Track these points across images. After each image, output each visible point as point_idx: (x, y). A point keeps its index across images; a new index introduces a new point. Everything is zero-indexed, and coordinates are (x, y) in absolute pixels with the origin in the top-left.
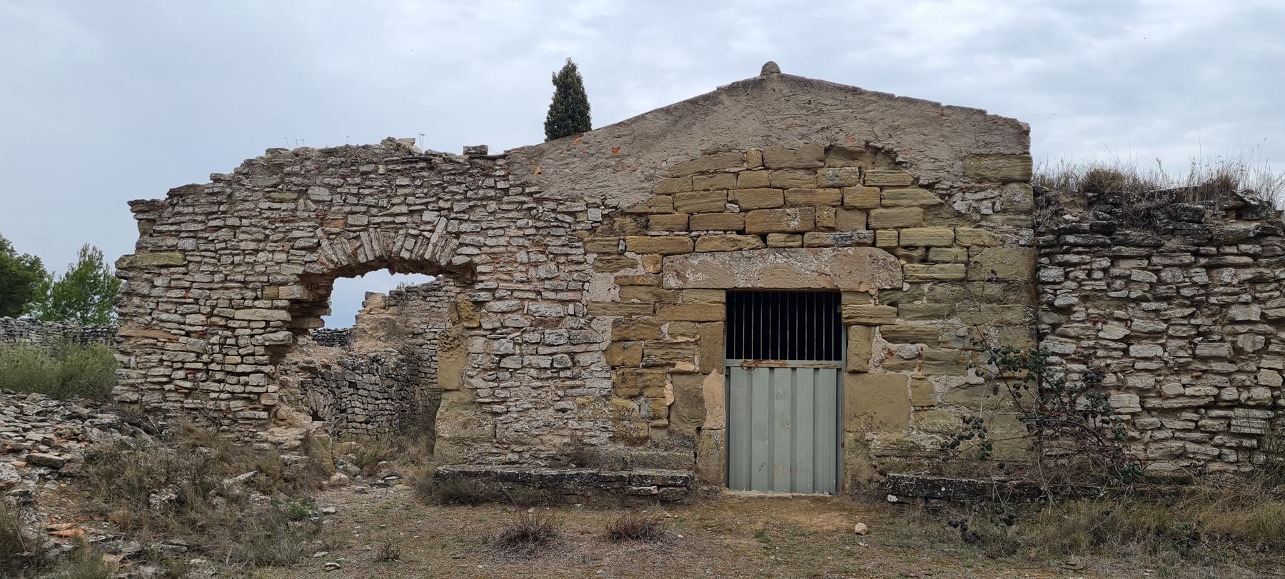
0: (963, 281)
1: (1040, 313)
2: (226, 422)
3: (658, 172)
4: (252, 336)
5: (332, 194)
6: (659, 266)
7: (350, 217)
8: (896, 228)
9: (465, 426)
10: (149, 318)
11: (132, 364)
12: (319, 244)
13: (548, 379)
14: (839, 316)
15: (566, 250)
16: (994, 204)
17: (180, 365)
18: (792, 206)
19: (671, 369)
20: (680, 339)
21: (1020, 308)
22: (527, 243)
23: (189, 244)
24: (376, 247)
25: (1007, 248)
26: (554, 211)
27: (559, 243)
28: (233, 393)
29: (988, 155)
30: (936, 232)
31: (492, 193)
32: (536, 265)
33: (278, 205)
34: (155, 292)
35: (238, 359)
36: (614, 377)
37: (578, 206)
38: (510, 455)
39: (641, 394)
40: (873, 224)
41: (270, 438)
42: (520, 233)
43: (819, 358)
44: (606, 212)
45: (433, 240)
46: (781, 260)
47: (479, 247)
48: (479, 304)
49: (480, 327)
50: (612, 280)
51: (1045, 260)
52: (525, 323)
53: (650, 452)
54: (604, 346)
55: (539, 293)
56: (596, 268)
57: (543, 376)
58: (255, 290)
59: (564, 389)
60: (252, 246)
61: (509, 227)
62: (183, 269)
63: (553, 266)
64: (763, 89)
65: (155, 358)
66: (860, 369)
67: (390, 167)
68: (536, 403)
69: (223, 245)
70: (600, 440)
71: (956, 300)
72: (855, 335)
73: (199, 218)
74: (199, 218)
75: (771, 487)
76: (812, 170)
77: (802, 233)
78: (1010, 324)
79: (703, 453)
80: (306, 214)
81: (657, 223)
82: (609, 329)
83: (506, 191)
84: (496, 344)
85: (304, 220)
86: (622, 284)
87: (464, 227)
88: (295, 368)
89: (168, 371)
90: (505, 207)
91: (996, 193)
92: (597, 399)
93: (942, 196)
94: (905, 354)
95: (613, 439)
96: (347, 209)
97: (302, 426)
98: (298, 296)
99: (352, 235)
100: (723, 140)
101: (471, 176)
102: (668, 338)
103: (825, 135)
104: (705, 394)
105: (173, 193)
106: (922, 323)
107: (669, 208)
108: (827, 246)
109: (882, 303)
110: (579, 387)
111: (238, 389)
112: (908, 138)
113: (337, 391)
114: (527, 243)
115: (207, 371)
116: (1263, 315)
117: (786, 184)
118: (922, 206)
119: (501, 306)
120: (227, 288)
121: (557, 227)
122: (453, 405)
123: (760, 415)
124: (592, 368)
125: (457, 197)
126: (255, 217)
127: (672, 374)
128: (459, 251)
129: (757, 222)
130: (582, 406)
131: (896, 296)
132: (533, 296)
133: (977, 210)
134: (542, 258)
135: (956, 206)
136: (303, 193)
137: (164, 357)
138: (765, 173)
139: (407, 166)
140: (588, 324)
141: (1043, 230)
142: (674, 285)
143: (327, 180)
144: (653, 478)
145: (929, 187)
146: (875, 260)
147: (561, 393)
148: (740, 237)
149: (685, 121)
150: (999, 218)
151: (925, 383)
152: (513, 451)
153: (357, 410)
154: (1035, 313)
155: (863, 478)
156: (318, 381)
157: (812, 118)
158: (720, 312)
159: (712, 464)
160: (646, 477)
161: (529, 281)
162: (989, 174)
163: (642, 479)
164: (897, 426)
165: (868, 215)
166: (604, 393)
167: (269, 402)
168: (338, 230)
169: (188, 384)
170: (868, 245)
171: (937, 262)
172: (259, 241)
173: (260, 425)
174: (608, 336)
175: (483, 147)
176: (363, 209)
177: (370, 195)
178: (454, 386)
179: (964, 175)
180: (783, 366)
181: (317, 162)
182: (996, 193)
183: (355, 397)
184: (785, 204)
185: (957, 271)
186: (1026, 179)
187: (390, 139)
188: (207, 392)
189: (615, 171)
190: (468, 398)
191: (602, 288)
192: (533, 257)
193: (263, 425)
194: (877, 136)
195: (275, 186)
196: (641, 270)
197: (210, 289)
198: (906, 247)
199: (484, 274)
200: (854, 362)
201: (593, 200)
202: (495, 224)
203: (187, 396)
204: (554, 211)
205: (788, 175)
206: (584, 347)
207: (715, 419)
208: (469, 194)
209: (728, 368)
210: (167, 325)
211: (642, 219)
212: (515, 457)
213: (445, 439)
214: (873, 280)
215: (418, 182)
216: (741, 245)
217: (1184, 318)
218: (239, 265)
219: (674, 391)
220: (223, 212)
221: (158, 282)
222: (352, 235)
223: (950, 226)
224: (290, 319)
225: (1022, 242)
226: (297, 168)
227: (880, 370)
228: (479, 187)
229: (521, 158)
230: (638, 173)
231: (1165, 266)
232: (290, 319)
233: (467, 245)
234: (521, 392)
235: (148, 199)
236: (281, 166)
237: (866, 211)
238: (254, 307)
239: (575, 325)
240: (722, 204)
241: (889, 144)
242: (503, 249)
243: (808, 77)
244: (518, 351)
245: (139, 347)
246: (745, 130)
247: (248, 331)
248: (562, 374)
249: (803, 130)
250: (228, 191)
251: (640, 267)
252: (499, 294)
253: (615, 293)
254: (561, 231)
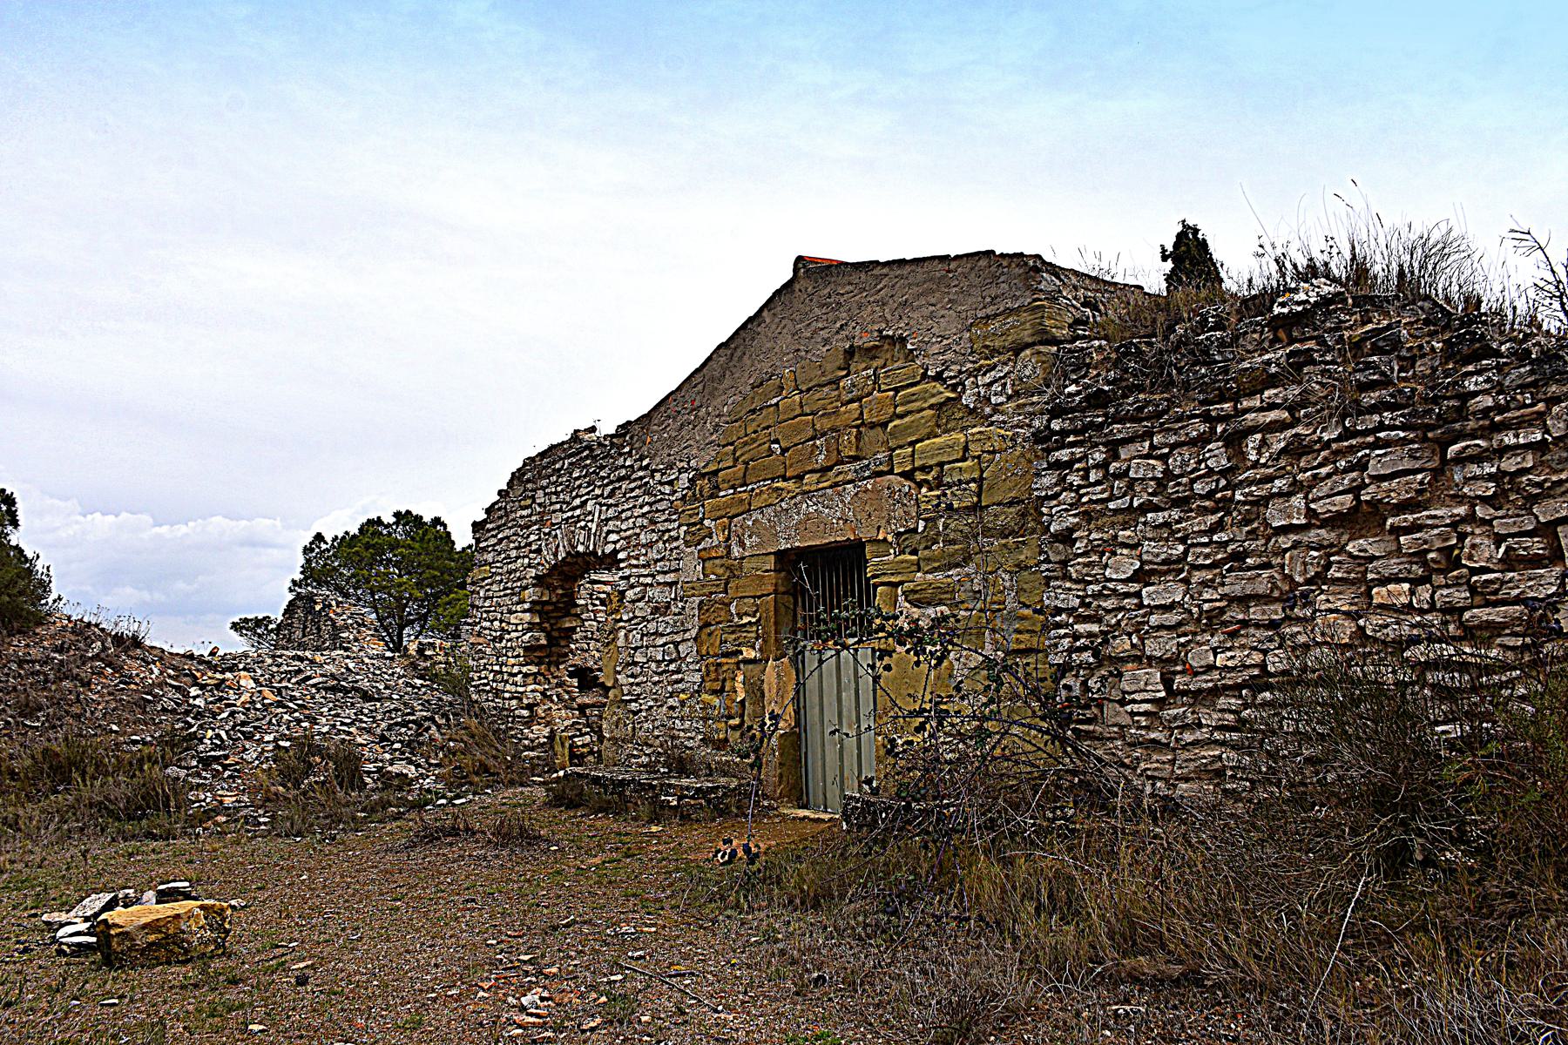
0: (976, 508)
29: (996, 315)
31: (623, 472)
93: (954, 388)
105: (488, 511)
116: (1311, 513)
118: (931, 407)
186: (1223, 297)
217: (1202, 533)
231: (1173, 447)
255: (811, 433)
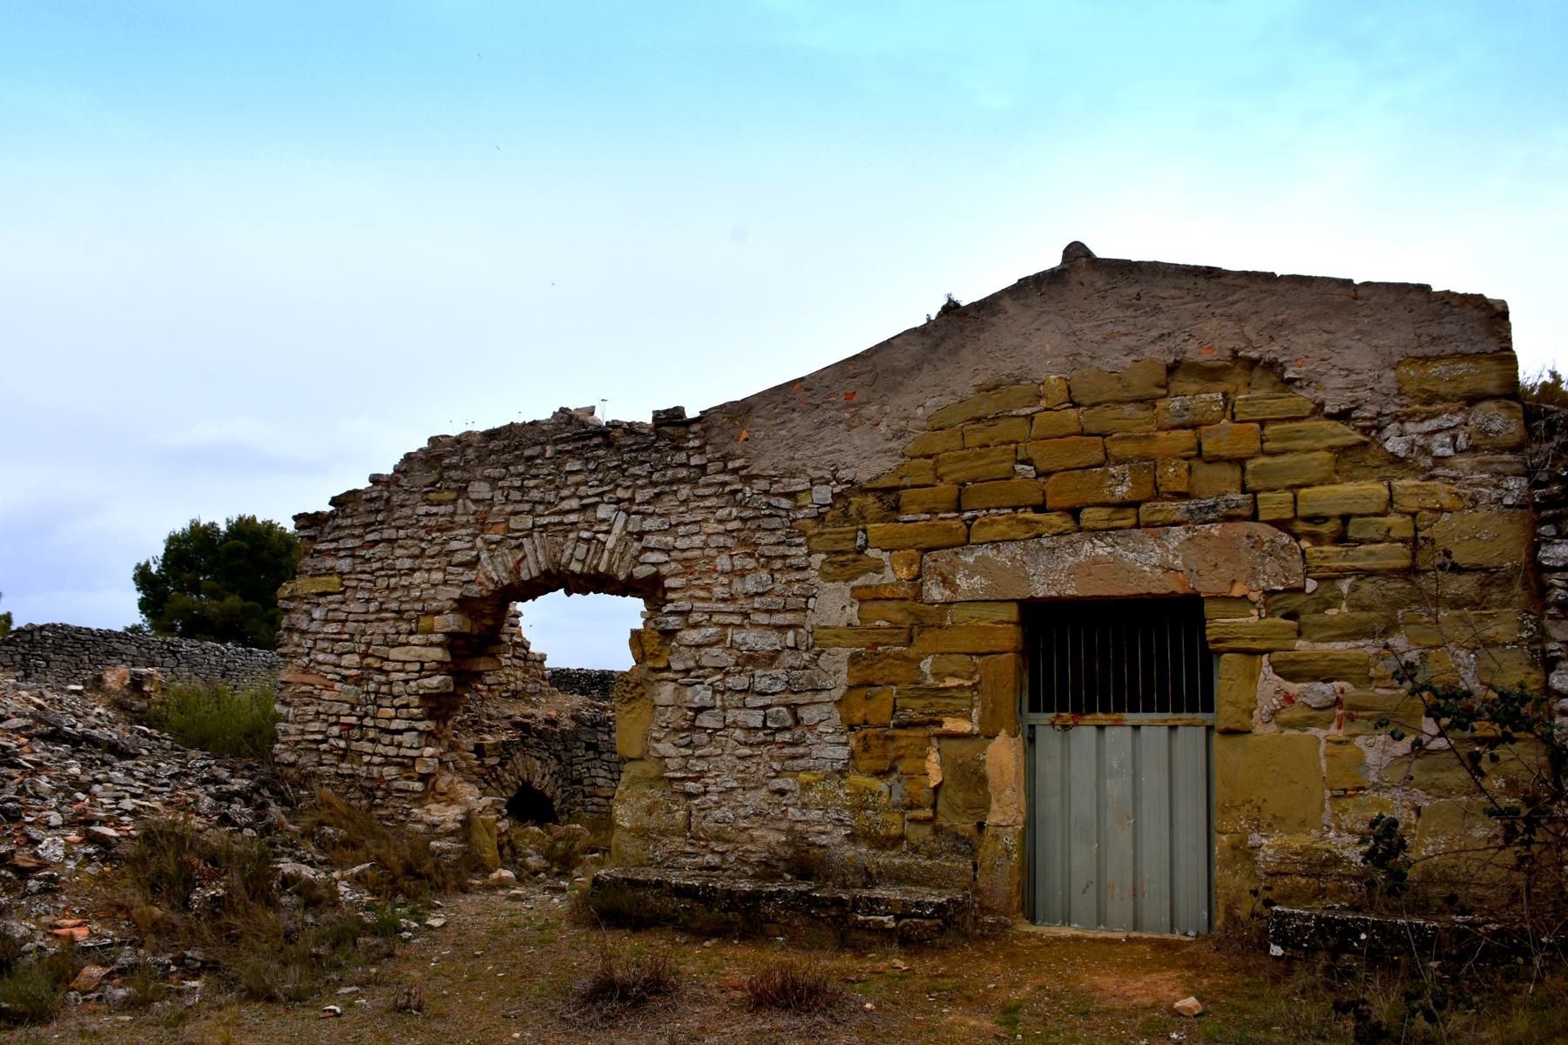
0: (1410, 572)
1: (1547, 622)
2: (380, 793)
3: (913, 423)
4: (407, 682)
5: (493, 490)
6: (915, 568)
7: (512, 519)
8: (1291, 488)
9: (649, 812)
10: (306, 659)
11: (291, 717)
12: (478, 558)
13: (759, 744)
14: (1204, 643)
15: (782, 550)
16: (1455, 438)
17: (333, 719)
18: (1119, 462)
19: (937, 730)
20: (951, 682)
21: (1511, 613)
22: (730, 542)
23: (344, 565)
24: (541, 559)
25: (1482, 513)
26: (766, 492)
27: (772, 539)
28: (386, 756)
30: (1361, 491)
31: (683, 473)
32: (742, 574)
33: (434, 510)
34: (314, 627)
35: (392, 712)
36: (853, 742)
37: (799, 484)
38: (709, 857)
39: (893, 769)
40: (1251, 484)
41: (427, 818)
42: (721, 528)
43: (1177, 709)
44: (837, 490)
45: (610, 545)
46: (1102, 550)
47: (667, 552)
48: (669, 634)
49: (668, 668)
50: (848, 593)
51: (1547, 530)
52: (728, 660)
53: (906, 860)
54: (837, 694)
55: (746, 615)
56: (825, 576)
57: (753, 740)
58: (409, 621)
59: (782, 760)
60: (408, 563)
61: (706, 520)
62: (339, 597)
63: (765, 575)
64: (1066, 283)
65: (311, 709)
66: (1237, 726)
67: (559, 447)
68: (744, 780)
69: (378, 565)
70: (832, 839)
71: (1396, 605)
72: (1228, 671)
73: (357, 532)
74: (357, 532)
75: (1101, 919)
76: (1147, 402)
77: (1136, 505)
78: (1495, 644)
79: (986, 864)
80: (464, 519)
81: (912, 502)
82: (844, 668)
83: (702, 468)
84: (689, 692)
85: (463, 526)
86: (865, 597)
87: (649, 524)
88: (506, 724)
89: (324, 727)
90: (700, 492)
91: (1457, 419)
92: (827, 777)
93: (1365, 431)
94: (1314, 701)
95: (852, 838)
96: (509, 508)
97: (466, 803)
98: (454, 628)
99: (514, 542)
100: (1008, 367)
101: (657, 451)
102: (931, 681)
103: (1165, 345)
104: (990, 770)
106: (1340, 646)
107: (928, 479)
108: (1176, 524)
109: (1271, 614)
110: (802, 756)
111: (392, 751)
112: (1301, 340)
113: (564, 756)
114: (730, 542)
115: (361, 727)
117: (1107, 427)
118: (1330, 449)
119: (693, 636)
120: (382, 620)
121: (770, 516)
122: (634, 781)
123: (1082, 802)
124: (821, 728)
125: (640, 482)
126: (412, 525)
127: (939, 737)
128: (641, 559)
129: (1062, 491)
130: (807, 787)
131: (1296, 602)
132: (736, 620)
133: (1426, 451)
134: (750, 563)
135: (1389, 446)
136: (462, 491)
137: (321, 709)
138: (1073, 413)
139: (579, 444)
140: (814, 661)
141: (1544, 477)
142: (938, 597)
143: (488, 472)
144: (888, 902)
145: (1343, 416)
146: (1257, 543)
147: (776, 766)
148: (1038, 517)
149: (949, 344)
150: (1465, 462)
151: (1348, 750)
152: (713, 852)
153: (600, 781)
154: (1538, 624)
155: (1242, 912)
156: (531, 741)
157: (1142, 321)
158: (1009, 637)
159: (1001, 882)
160: (878, 901)
161: (733, 598)
162: (1442, 389)
163: (872, 905)
164: (1303, 823)
165: (1243, 470)
166: (838, 766)
167: (424, 770)
168: (498, 537)
169: (342, 744)
170: (1246, 519)
171: (1361, 542)
172: (415, 557)
173: (415, 800)
174: (843, 678)
175: (676, 408)
176: (527, 507)
177: (536, 487)
178: (636, 753)
179: (1400, 393)
180: (1118, 723)
181: (477, 449)
182: (1457, 419)
183: (598, 763)
184: (1107, 460)
185: (1396, 556)
186: (1511, 390)
187: (563, 410)
188: (361, 754)
189: (850, 428)
190: (654, 772)
191: (834, 605)
192: (738, 563)
193: (420, 800)
194: (1249, 342)
195: (433, 484)
196: (889, 576)
197: (366, 622)
198: (1310, 519)
199: (674, 590)
200: (1225, 714)
201: (820, 473)
202: (688, 518)
203: (343, 758)
204: (766, 492)
205: (1110, 414)
206: (808, 697)
207: (1005, 812)
208: (655, 476)
209: (1032, 727)
210: (323, 668)
211: (890, 497)
212: (716, 860)
213: (625, 829)
214: (1253, 577)
215: (592, 466)
216: (1040, 529)
218: (395, 589)
219: (942, 764)
220: (381, 523)
221: (317, 614)
222: (514, 542)
223: (1381, 479)
224: (448, 659)
225: (1508, 501)
226: (454, 460)
227: (1273, 728)
228: (667, 466)
229: (721, 420)
230: (882, 428)
232: (448, 659)
233: (652, 550)
234: (723, 765)
235: (311, 511)
236: (439, 458)
237: (1239, 462)
238: (407, 644)
239: (797, 663)
240: (1008, 465)
241: (1272, 351)
242: (697, 553)
243: (1134, 259)
244: (719, 703)
245: (297, 695)
246: (1042, 353)
247: (402, 676)
248: (779, 738)
249: (1131, 341)
250: (386, 494)
251: (888, 572)
252: (695, 617)
253: (852, 612)
254: (776, 523)
255: (1100, 457)
